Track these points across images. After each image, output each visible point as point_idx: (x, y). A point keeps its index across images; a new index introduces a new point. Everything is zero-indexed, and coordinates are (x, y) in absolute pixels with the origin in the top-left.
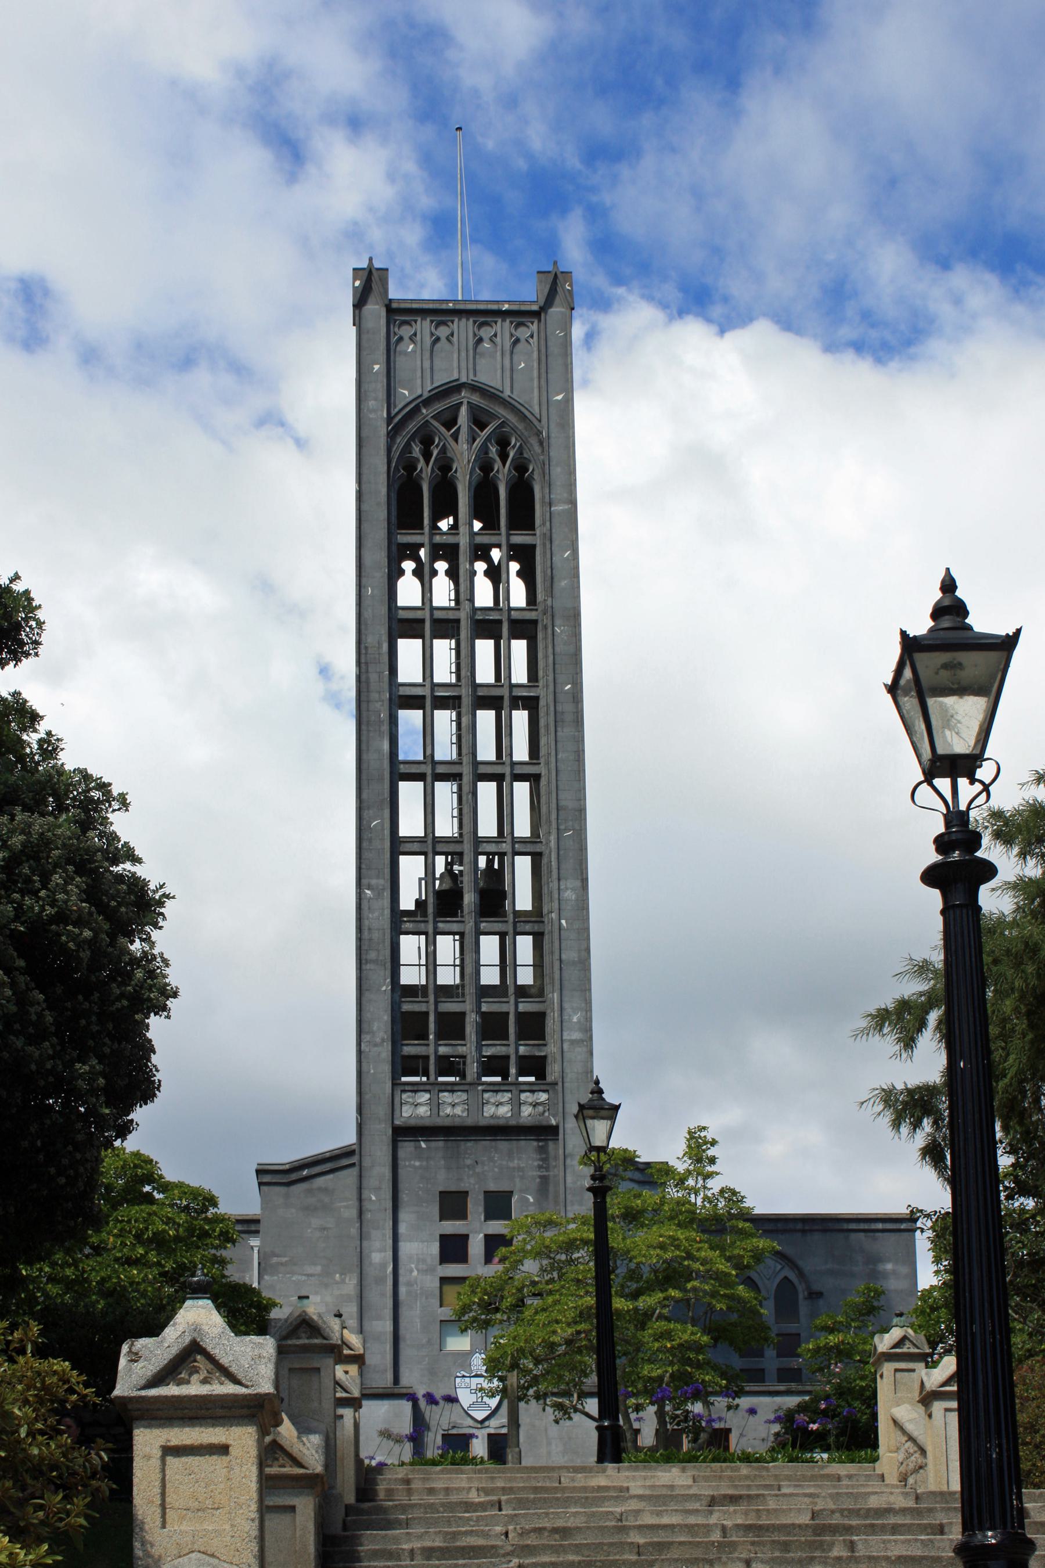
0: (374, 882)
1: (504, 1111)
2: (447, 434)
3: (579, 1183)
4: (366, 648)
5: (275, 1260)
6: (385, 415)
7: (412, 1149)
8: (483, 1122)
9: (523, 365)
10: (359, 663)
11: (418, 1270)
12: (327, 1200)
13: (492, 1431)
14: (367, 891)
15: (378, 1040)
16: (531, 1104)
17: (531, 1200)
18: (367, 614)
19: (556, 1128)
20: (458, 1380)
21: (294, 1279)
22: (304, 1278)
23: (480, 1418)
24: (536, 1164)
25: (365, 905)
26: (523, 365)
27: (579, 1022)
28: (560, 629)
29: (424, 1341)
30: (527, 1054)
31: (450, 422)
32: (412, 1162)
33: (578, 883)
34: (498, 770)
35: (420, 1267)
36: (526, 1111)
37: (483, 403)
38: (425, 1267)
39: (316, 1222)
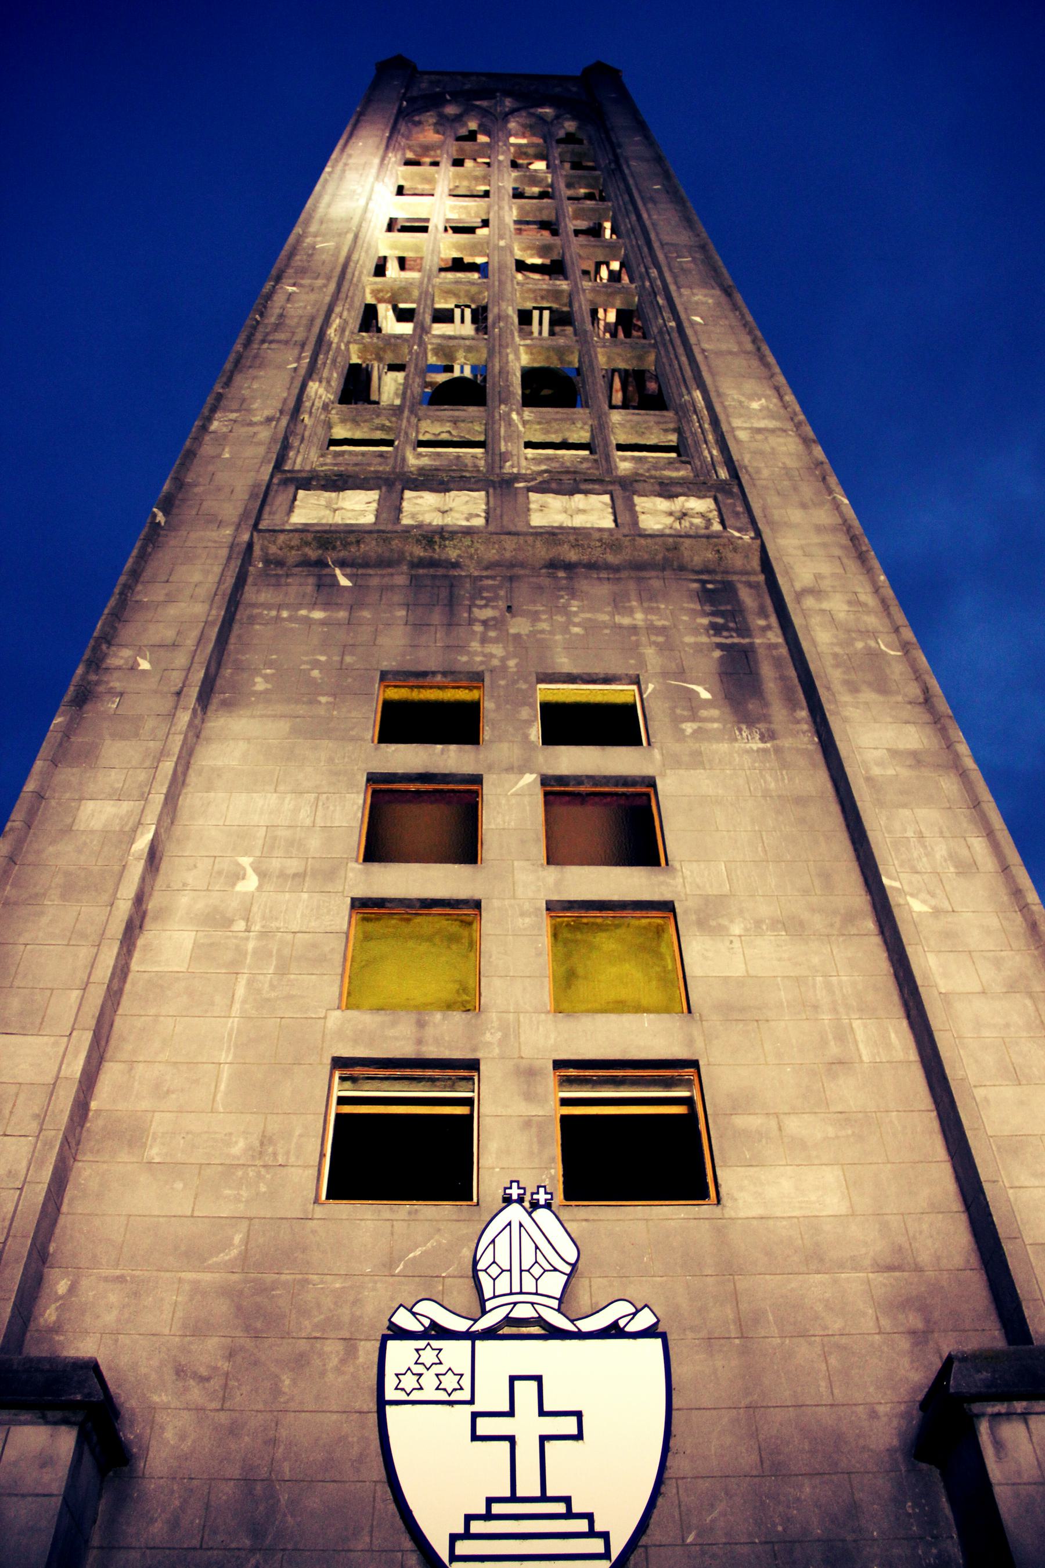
3: (859, 645)
11: (263, 875)
17: (705, 695)
20: (399, 1353)
24: (705, 621)
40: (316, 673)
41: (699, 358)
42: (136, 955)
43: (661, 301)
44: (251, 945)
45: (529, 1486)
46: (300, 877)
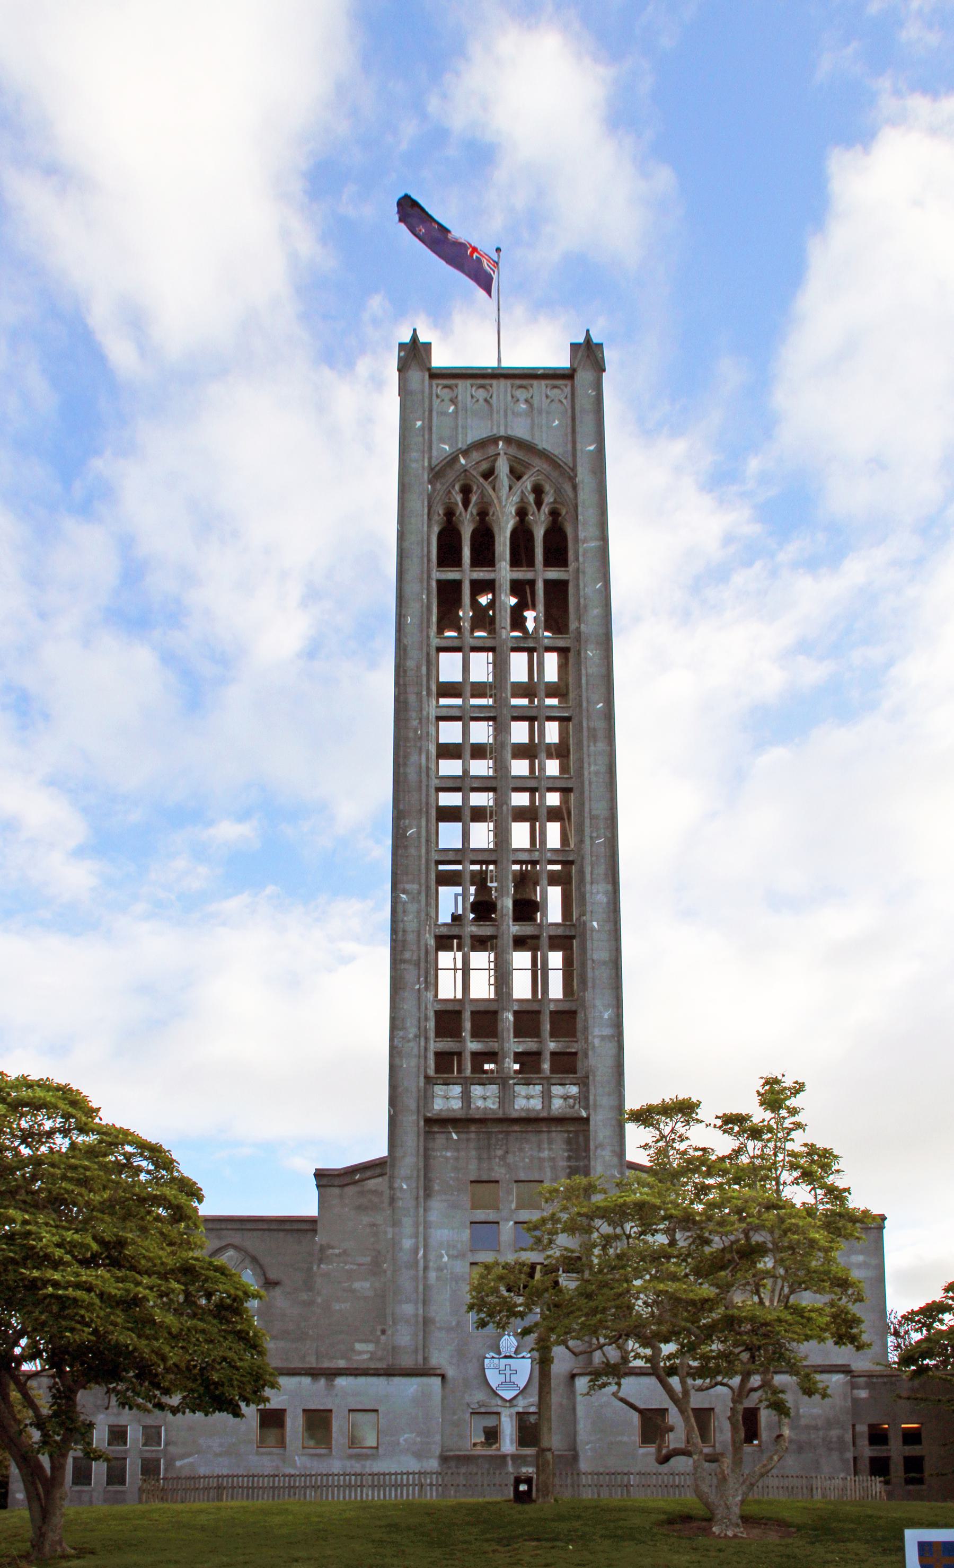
0: (408, 887)
1: (536, 1104)
2: (486, 484)
4: (405, 671)
5: (331, 1251)
6: (426, 464)
7: (444, 1141)
8: (514, 1115)
9: (557, 422)
10: (397, 684)
11: (448, 1255)
12: (376, 1200)
13: (521, 1410)
14: (402, 895)
15: (411, 1036)
16: (562, 1097)
18: (407, 641)
19: (587, 1120)
21: (346, 1267)
22: (355, 1267)
23: (508, 1398)
24: (566, 1154)
25: (400, 909)
26: (557, 422)
27: (610, 1018)
28: (592, 652)
29: (454, 1323)
30: (558, 1050)
31: (489, 474)
32: (444, 1153)
33: (610, 887)
34: (533, 784)
35: (451, 1252)
36: (557, 1104)
37: (521, 455)
38: (455, 1253)
39: (366, 1219)
40: (451, 1182)
41: (439, 461)
42: (580, 528)
43: (424, 597)
44: (449, 1276)
45: (508, 1380)
46: (457, 1257)
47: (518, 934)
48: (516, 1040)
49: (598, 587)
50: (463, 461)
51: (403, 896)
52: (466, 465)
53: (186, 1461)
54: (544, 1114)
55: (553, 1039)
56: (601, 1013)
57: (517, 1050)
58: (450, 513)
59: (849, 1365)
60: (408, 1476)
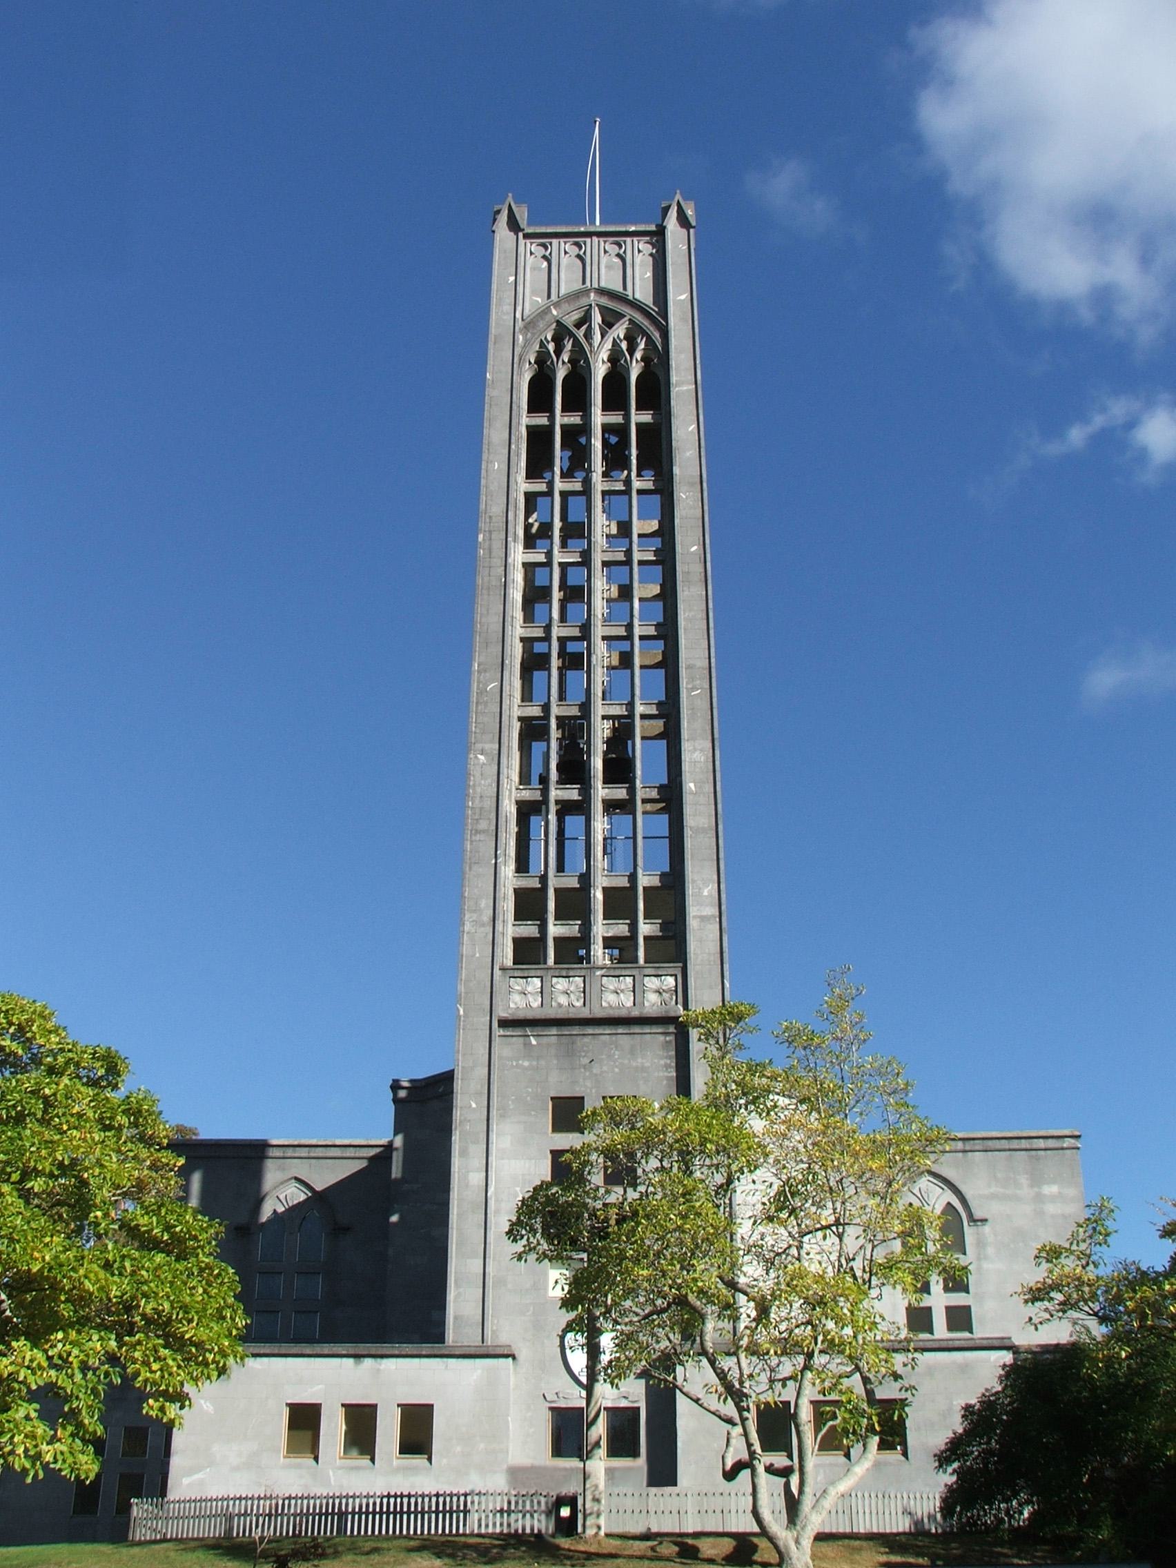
24: (662, 1062)
27: (710, 895)
36: (652, 998)
47: (607, 798)
48: (605, 922)
49: (690, 429)
50: (555, 312)
51: (481, 757)
52: (558, 316)
53: (196, 1477)
54: (635, 1013)
55: (647, 921)
56: (700, 889)
57: (606, 935)
58: (542, 360)
59: (1010, 1338)
60: (347, 1500)
